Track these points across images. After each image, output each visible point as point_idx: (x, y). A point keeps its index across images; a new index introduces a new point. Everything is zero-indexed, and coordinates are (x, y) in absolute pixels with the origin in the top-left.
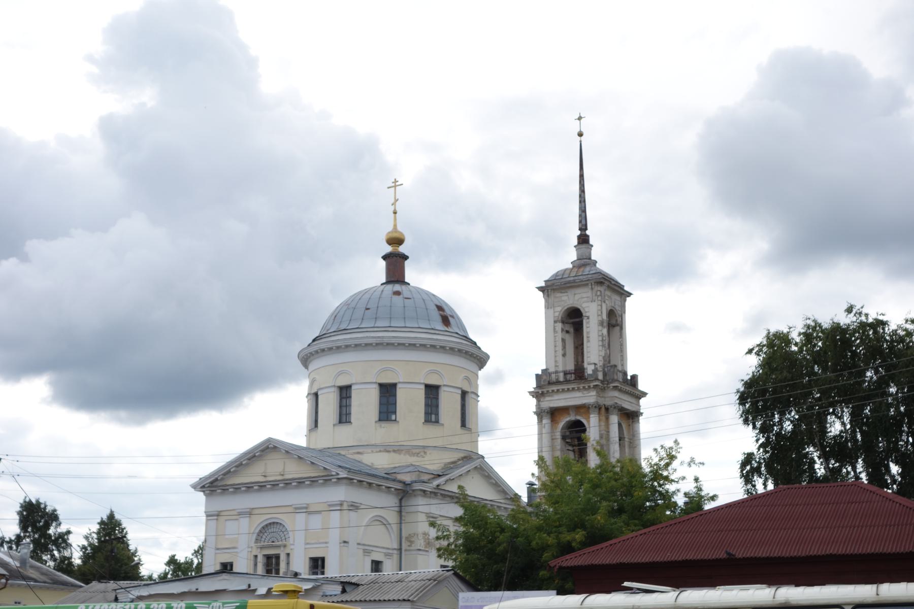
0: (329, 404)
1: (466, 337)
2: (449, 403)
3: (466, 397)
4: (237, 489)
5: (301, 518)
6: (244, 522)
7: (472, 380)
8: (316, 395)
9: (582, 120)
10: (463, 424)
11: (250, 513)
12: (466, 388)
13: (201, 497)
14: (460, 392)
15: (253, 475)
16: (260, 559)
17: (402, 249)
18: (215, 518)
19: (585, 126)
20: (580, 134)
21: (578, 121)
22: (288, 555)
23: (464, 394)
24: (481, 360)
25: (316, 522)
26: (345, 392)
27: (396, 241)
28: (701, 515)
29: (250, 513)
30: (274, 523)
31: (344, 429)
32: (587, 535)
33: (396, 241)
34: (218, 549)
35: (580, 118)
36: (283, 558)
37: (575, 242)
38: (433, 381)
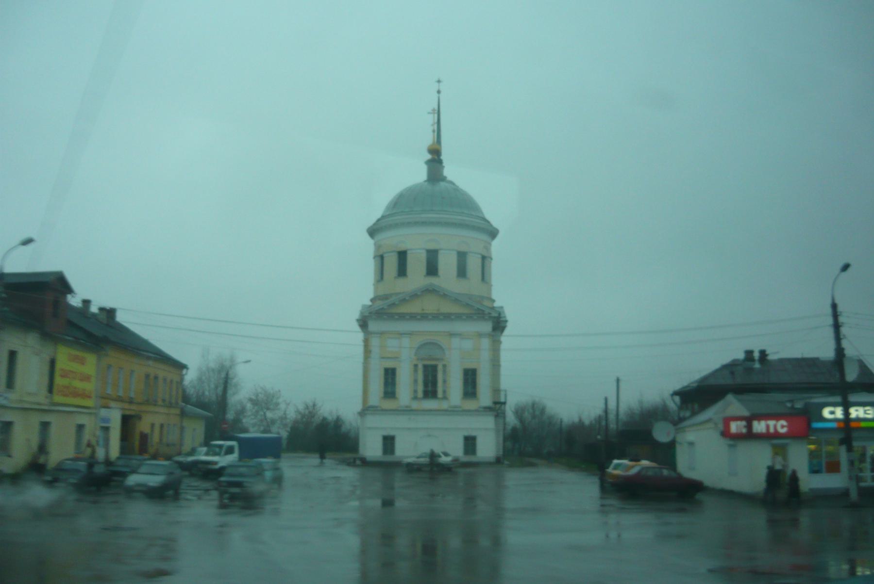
0: (391, 263)
1: (483, 218)
2: (474, 264)
3: (485, 259)
4: (402, 317)
5: (456, 342)
6: (406, 341)
7: (487, 248)
8: (382, 257)
9: (441, 84)
10: (483, 278)
11: (411, 334)
12: (486, 254)
14: (480, 256)
15: (414, 308)
16: (420, 367)
18: (409, 336)
19: (442, 87)
20: (439, 92)
21: (437, 84)
22: (444, 366)
23: (484, 258)
24: (493, 233)
25: (468, 345)
26: (402, 256)
28: (131, 402)
29: (411, 334)
30: (439, 345)
31: (401, 281)
32: (274, 401)
34: (383, 358)
35: (439, 81)
36: (440, 368)
38: (463, 248)
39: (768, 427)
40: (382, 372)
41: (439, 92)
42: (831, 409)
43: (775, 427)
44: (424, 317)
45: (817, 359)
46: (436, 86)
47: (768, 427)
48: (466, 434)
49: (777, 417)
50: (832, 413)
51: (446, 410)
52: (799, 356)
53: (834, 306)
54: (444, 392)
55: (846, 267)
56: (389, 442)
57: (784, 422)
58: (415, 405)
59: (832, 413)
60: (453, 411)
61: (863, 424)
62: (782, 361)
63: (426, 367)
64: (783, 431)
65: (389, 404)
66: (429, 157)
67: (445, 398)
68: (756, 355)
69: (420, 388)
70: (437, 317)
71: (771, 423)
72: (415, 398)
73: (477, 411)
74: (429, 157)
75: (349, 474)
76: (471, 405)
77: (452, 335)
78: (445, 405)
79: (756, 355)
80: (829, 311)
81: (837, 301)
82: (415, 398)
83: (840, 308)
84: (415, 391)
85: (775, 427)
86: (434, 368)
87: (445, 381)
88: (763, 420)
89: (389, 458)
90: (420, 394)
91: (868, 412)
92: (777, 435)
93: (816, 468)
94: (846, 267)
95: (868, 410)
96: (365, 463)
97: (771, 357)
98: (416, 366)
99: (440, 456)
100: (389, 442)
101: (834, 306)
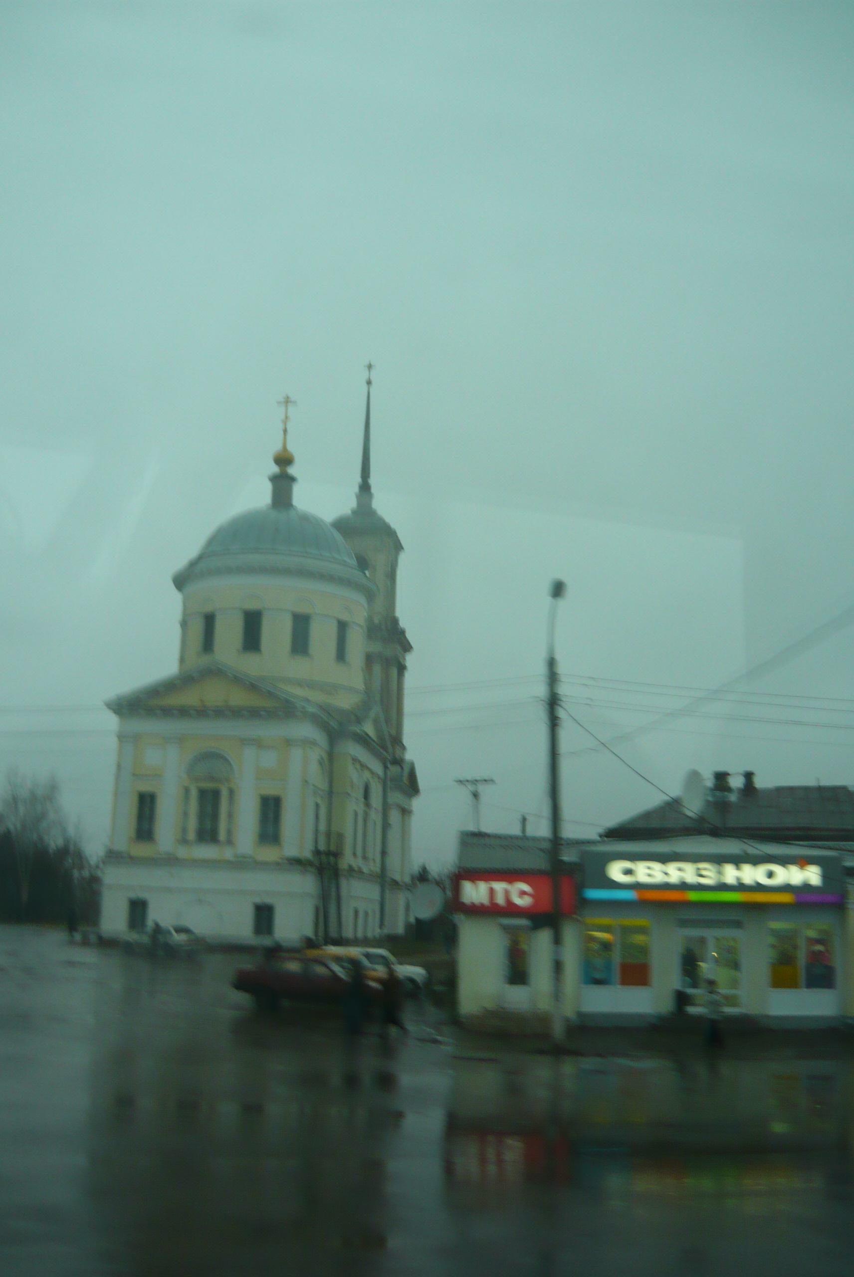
5: (249, 753)
13: (112, 721)
15: (189, 698)
16: (194, 793)
17: (292, 471)
20: (369, 383)
22: (231, 792)
25: (269, 759)
27: (284, 460)
33: (284, 460)
35: (370, 367)
36: (225, 793)
37: (356, 489)
38: (301, 609)
39: (492, 891)
40: (135, 799)
41: (369, 383)
42: (627, 864)
43: (507, 893)
44: (202, 712)
45: (844, 789)
46: (365, 375)
47: (492, 891)
48: (258, 900)
49: (510, 875)
50: (628, 872)
51: (229, 862)
52: (811, 782)
53: (552, 663)
54: (229, 832)
55: (558, 590)
56: (138, 908)
57: (525, 887)
58: (182, 852)
59: (628, 872)
60: (241, 864)
61: (693, 896)
62: (780, 790)
63: (202, 793)
64: (521, 902)
65: (142, 850)
66: (275, 469)
67: (230, 842)
68: (736, 782)
69: (192, 824)
70: (222, 712)
71: (499, 887)
72: (184, 841)
73: (278, 864)
74: (275, 469)
75: (89, 956)
76: (269, 854)
77: (244, 742)
78: (228, 854)
79: (736, 782)
80: (541, 669)
81: (558, 657)
82: (184, 841)
83: (562, 669)
84: (184, 830)
85: (507, 893)
86: (216, 794)
87: (230, 816)
88: (481, 880)
89: (266, 941)
90: (192, 835)
91: (704, 873)
92: (511, 910)
93: (598, 976)
94: (558, 590)
95: (705, 869)
96: (106, 944)
97: (759, 783)
98: (187, 790)
99: (169, 932)
100: (138, 908)
101: (552, 663)
